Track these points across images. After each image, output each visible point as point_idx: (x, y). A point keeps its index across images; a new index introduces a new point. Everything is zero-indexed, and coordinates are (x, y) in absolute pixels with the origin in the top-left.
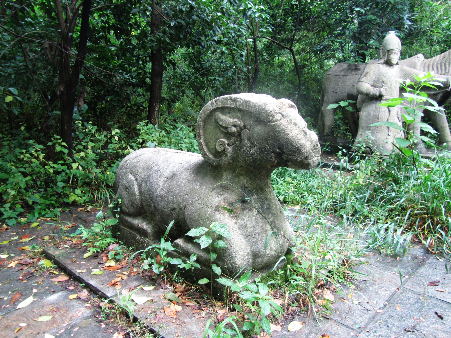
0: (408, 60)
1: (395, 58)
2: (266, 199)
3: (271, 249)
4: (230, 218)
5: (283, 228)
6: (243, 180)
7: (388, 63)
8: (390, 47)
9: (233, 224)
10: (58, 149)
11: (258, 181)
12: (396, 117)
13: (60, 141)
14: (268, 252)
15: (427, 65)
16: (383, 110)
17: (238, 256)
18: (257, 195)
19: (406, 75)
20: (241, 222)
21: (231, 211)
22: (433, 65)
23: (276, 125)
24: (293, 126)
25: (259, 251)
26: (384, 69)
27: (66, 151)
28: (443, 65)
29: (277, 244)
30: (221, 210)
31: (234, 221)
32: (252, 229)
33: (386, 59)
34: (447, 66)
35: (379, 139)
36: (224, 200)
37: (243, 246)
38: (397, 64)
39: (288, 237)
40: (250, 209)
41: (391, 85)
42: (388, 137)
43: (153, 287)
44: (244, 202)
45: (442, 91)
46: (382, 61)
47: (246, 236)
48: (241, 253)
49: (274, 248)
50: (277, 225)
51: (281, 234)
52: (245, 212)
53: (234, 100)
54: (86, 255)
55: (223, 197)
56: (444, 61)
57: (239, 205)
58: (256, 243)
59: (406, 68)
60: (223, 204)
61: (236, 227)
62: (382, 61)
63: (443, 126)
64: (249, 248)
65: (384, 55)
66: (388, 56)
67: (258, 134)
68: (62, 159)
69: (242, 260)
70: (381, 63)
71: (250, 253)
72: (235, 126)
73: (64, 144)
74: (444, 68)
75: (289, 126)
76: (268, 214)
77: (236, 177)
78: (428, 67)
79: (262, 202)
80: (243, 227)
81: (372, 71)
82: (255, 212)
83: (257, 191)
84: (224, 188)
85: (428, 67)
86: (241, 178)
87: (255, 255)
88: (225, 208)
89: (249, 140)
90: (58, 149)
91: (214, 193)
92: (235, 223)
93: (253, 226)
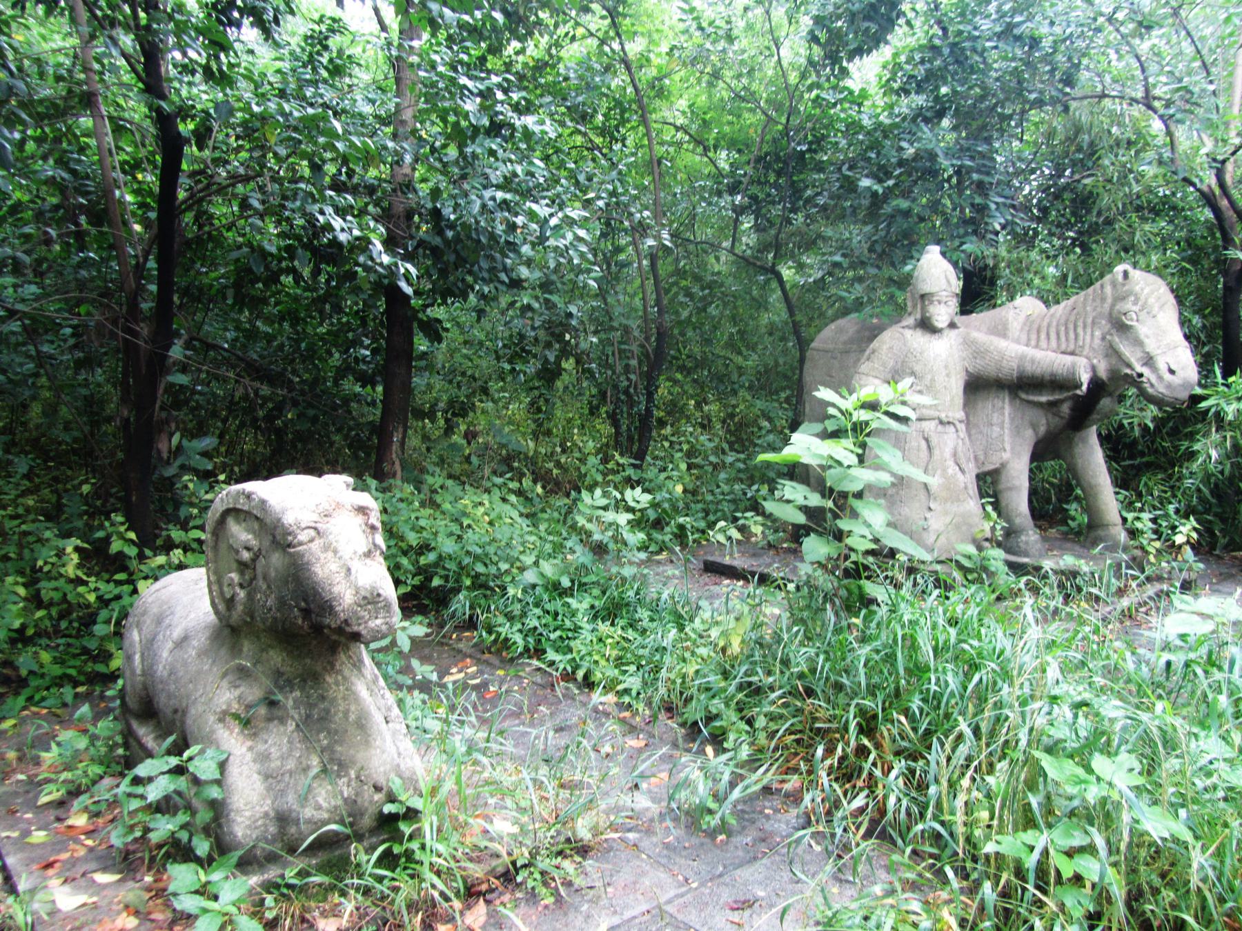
0: (981, 318)
1: (943, 313)
2: (323, 698)
3: (319, 808)
4: (241, 738)
5: (354, 763)
6: (276, 658)
7: (926, 325)
8: (926, 288)
9: (244, 749)
10: (116, 546)
11: (308, 661)
12: (951, 463)
13: (122, 529)
14: (308, 812)
15: (1035, 326)
16: (914, 444)
17: (239, 819)
18: (302, 689)
19: (977, 351)
20: (261, 747)
21: (246, 723)
22: (1049, 326)
23: (298, 553)
24: (330, 554)
25: (290, 811)
26: (918, 339)
27: (132, 551)
28: (1071, 326)
29: (335, 797)
30: (228, 718)
31: (249, 743)
32: (278, 763)
33: (918, 316)
34: (1080, 330)
35: (907, 519)
36: (240, 697)
37: (255, 798)
38: (952, 325)
39: (382, 781)
40: (282, 721)
41: (933, 380)
42: (928, 515)
43: (118, 877)
44: (272, 704)
45: (1066, 394)
46: (910, 321)
47: (267, 777)
48: (247, 814)
49: (325, 805)
50: (337, 756)
51: (347, 775)
52: (271, 725)
53: (248, 496)
54: (44, 800)
55: (237, 692)
56: (1072, 318)
57: (263, 711)
58: (283, 792)
59: (980, 337)
60: (235, 707)
61: (249, 756)
62: (910, 321)
63: (1093, 482)
64: (269, 802)
65: (914, 306)
66: (924, 310)
67: (276, 570)
68: (124, 569)
69: (249, 827)
70: (908, 327)
71: (272, 814)
72: (248, 549)
73: (132, 535)
74: (1072, 335)
75: (322, 556)
76: (319, 732)
77: (262, 650)
78: (1038, 332)
79: (311, 706)
80: (263, 758)
81: (885, 347)
82: (291, 726)
83: (304, 681)
84: (243, 674)
85: (1038, 332)
86: (271, 653)
87: (283, 819)
88: (236, 716)
89: (265, 578)
90: (116, 546)
91: (225, 683)
92: (250, 749)
93: (282, 758)
